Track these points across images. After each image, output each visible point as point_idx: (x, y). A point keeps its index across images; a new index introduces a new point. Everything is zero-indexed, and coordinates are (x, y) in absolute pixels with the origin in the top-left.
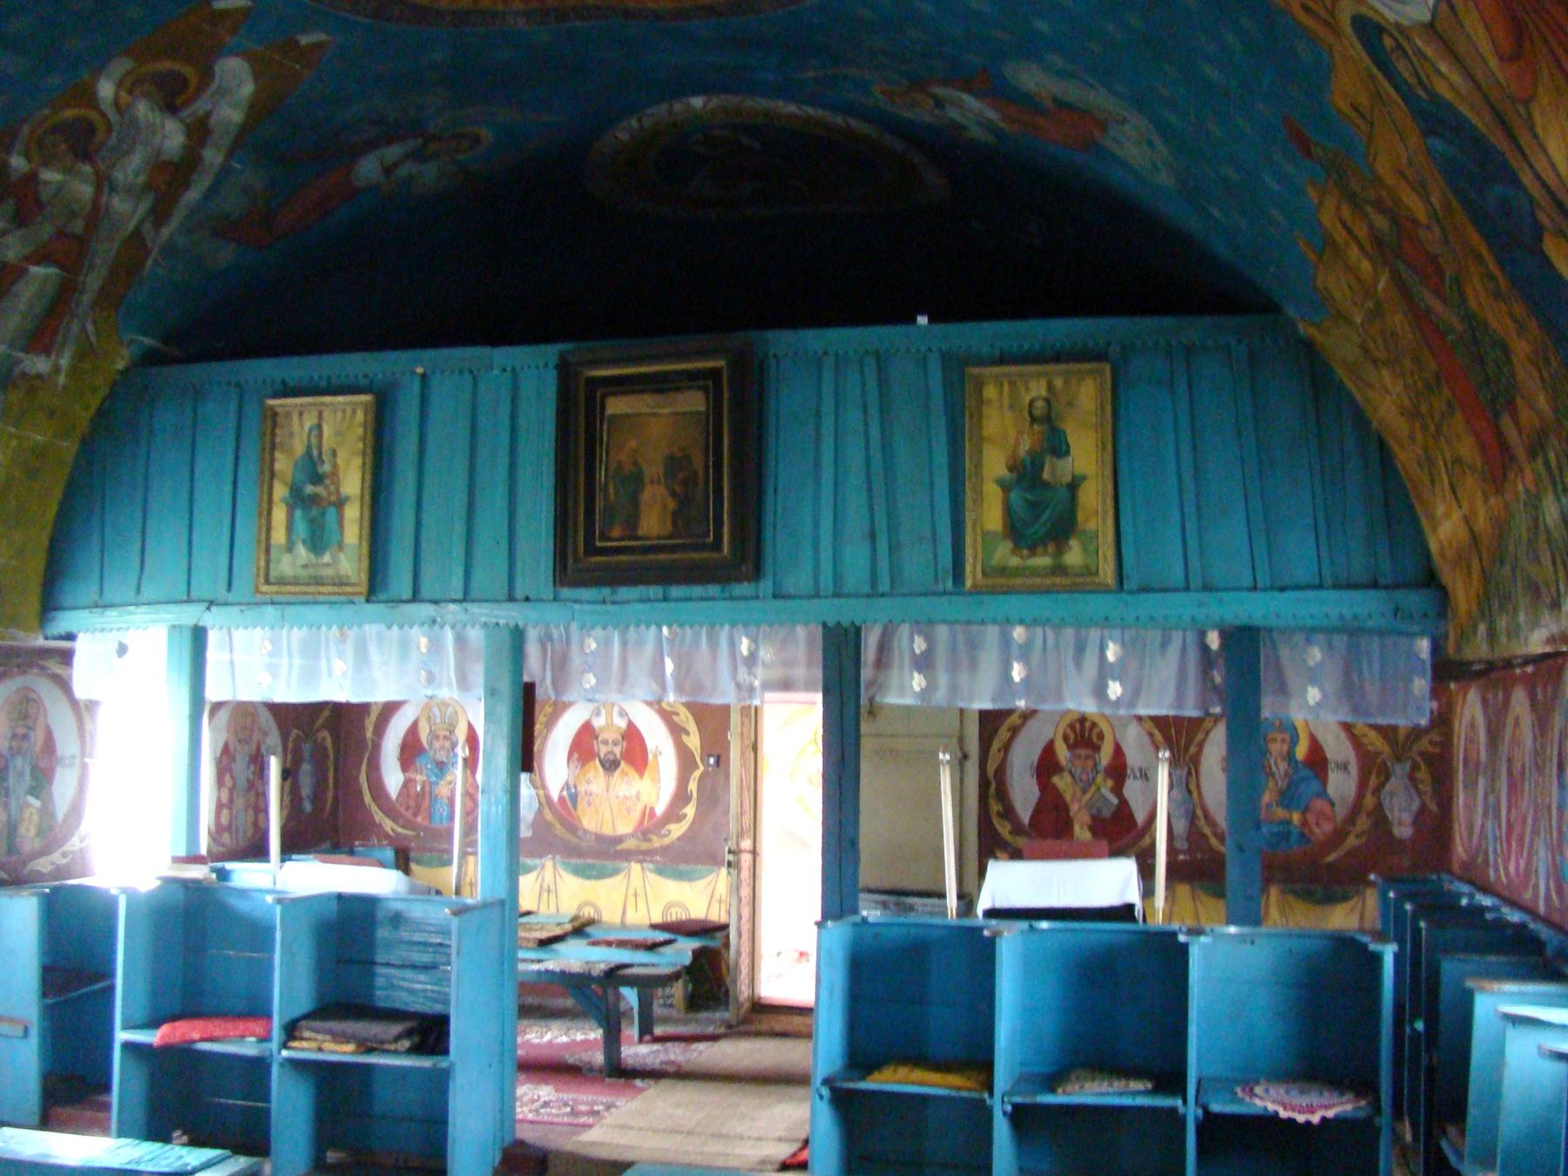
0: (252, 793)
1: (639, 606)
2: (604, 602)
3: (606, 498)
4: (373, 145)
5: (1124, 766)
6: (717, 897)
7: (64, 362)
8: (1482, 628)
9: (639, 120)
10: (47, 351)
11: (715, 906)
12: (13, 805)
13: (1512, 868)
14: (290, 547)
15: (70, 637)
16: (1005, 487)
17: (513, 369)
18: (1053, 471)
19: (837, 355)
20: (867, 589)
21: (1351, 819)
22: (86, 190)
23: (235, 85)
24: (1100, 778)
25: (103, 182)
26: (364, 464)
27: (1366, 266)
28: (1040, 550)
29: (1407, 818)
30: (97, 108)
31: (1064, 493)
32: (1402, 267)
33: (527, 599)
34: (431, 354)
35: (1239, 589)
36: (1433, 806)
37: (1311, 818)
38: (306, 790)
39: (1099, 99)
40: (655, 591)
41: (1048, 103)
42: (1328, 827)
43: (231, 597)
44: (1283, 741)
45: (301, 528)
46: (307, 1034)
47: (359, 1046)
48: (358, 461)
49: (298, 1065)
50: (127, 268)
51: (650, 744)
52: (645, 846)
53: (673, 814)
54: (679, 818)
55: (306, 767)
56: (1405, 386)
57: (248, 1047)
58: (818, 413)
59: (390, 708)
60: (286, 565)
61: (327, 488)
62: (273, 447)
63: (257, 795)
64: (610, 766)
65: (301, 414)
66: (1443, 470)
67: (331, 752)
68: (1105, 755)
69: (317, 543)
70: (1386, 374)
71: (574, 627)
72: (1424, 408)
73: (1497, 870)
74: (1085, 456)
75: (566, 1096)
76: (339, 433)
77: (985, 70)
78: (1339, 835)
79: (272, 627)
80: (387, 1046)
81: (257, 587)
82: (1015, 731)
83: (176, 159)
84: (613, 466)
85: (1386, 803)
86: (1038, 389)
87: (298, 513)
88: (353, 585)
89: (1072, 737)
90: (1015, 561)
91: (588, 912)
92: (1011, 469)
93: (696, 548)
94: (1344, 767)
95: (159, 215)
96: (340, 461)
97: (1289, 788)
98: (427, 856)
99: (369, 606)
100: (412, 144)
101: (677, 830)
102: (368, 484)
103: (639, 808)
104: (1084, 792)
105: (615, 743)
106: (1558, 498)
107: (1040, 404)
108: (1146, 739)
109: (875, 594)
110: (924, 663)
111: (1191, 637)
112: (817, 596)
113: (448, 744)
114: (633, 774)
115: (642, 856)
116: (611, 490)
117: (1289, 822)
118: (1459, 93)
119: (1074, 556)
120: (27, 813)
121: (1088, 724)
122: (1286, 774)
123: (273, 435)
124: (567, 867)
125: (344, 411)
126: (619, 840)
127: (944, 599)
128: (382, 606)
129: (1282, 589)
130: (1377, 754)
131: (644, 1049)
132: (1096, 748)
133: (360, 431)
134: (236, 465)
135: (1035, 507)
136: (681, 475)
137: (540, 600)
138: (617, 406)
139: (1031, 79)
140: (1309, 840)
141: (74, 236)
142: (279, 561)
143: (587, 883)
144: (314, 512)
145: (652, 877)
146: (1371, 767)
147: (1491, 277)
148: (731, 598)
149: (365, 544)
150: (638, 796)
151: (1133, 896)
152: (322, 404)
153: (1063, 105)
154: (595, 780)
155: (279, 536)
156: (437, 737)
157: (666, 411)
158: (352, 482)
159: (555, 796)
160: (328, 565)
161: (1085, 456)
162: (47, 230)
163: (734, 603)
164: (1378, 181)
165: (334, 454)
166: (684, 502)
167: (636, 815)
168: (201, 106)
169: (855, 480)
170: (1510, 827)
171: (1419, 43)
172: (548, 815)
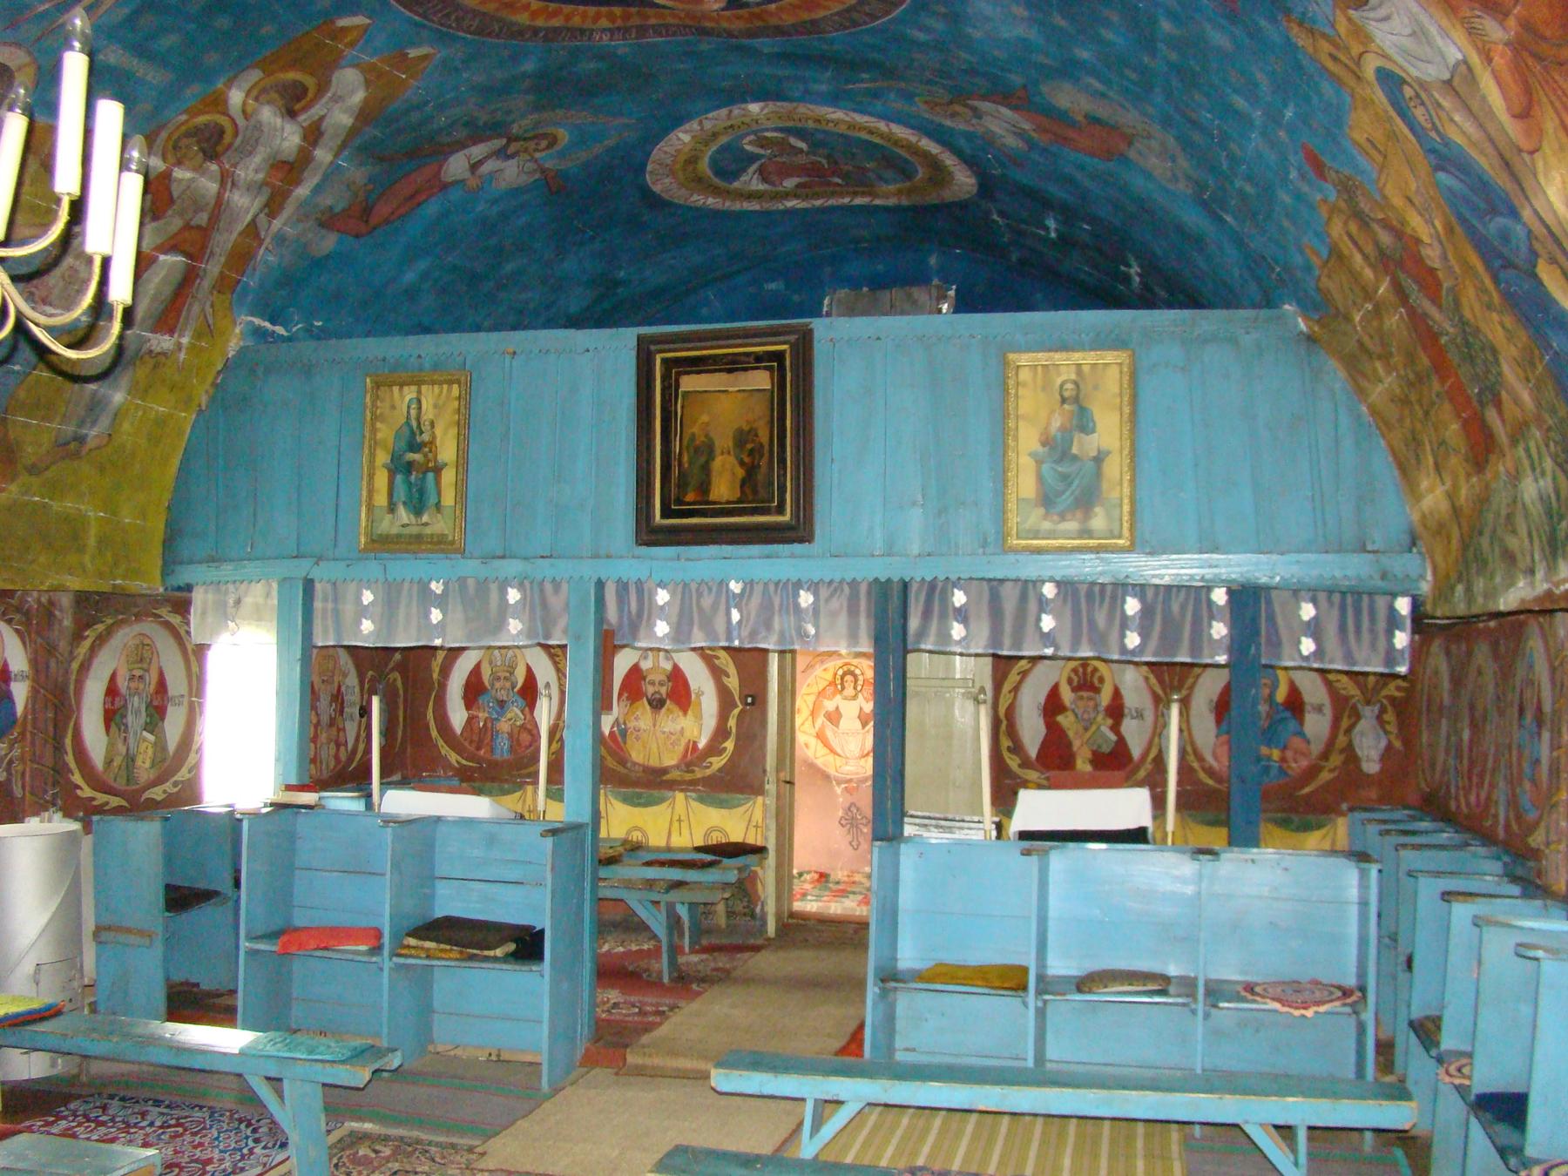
0: (334, 729)
3: (680, 465)
4: (461, 145)
7: (185, 341)
8: (1460, 588)
9: (701, 123)
10: (171, 332)
11: (752, 831)
12: (131, 741)
13: (1473, 798)
14: (392, 508)
15: (189, 588)
16: (1039, 462)
21: (1325, 756)
22: (213, 187)
23: (347, 95)
24: (1100, 718)
25: (226, 179)
27: (1368, 274)
28: (1069, 516)
29: (1375, 754)
30: (226, 113)
32: (1402, 276)
36: (1397, 744)
37: (1289, 754)
39: (1129, 118)
41: (1080, 118)
42: (1304, 763)
50: (241, 258)
51: (693, 686)
52: (688, 777)
53: (714, 748)
54: (721, 752)
56: (1398, 376)
59: (455, 653)
63: (339, 730)
64: (657, 704)
66: (1428, 448)
68: (1105, 697)
70: (1378, 365)
72: (1413, 398)
73: (1457, 799)
74: (1108, 432)
75: (632, 999)
77: (1025, 87)
78: (1312, 772)
82: (1024, 674)
83: (291, 159)
85: (1356, 742)
89: (1076, 679)
91: (636, 836)
92: (1044, 444)
95: (273, 207)
100: (498, 143)
101: (717, 762)
103: (683, 742)
104: (1086, 729)
105: (661, 684)
106: (1536, 480)
107: (1069, 386)
113: (508, 685)
114: (678, 712)
115: (686, 786)
116: (685, 458)
117: (1269, 758)
118: (1469, 138)
119: (1098, 522)
120: (143, 746)
121: (1089, 669)
126: (665, 771)
130: (1346, 699)
131: (695, 958)
132: (1097, 690)
136: (749, 446)
138: (689, 383)
139: (1067, 98)
140: (1286, 774)
141: (199, 227)
143: (637, 810)
145: (694, 804)
146: (1344, 710)
147: (1486, 291)
150: (682, 731)
153: (1094, 121)
154: (643, 717)
156: (499, 679)
159: (607, 731)
161: (1108, 432)
162: (176, 224)
164: (1386, 204)
165: (432, 424)
166: (751, 470)
167: (680, 749)
168: (317, 111)
170: (1472, 764)
171: (1437, 95)
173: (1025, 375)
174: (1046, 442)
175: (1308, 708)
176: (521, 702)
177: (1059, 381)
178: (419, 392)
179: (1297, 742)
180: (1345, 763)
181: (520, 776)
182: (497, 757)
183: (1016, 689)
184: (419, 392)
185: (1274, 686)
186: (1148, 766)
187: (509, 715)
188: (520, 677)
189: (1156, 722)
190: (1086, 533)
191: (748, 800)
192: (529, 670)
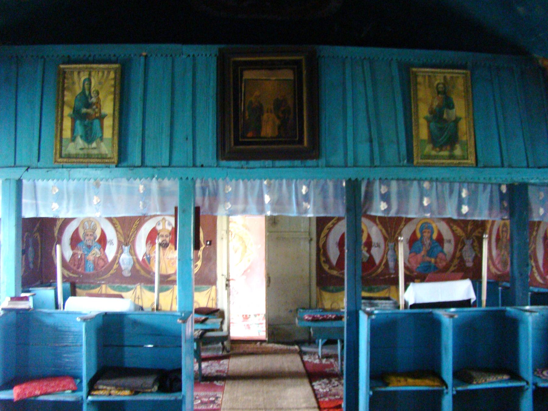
1: (260, 170)
2: (242, 168)
3: (244, 117)
5: (371, 242)
6: (211, 298)
14: (73, 139)
16: (429, 122)
17: (194, 55)
18: (448, 114)
19: (351, 58)
20: (368, 164)
26: (115, 99)
28: (444, 148)
29: (471, 259)
31: (452, 124)
33: (202, 166)
34: (152, 47)
35: (522, 167)
37: (438, 260)
38: (31, 259)
40: (268, 163)
42: (444, 264)
43: (39, 165)
44: (428, 232)
45: (80, 129)
46: (101, 387)
47: (131, 391)
48: (111, 97)
49: (93, 403)
55: (31, 249)
57: (68, 396)
58: (344, 84)
59: (67, 221)
60: (71, 148)
61: (94, 110)
62: (63, 90)
65: (79, 73)
67: (39, 242)
69: (89, 137)
71: (221, 182)
74: (460, 109)
76: (100, 83)
79: (58, 180)
80: (147, 390)
81: (55, 159)
84: (247, 105)
85: (464, 254)
86: (439, 80)
87: (78, 122)
88: (109, 158)
90: (433, 153)
93: (290, 143)
94: (449, 241)
96: (101, 96)
97: (430, 249)
98: (83, 285)
99: (117, 169)
102: (117, 108)
107: (441, 86)
108: (379, 232)
109: (372, 165)
110: (386, 198)
111: (495, 188)
112: (346, 166)
113: (92, 238)
117: (430, 262)
119: (458, 152)
122: (430, 244)
123: (64, 83)
124: (146, 288)
125: (103, 73)
126: (169, 276)
127: (404, 169)
128: (125, 169)
129: (539, 168)
130: (460, 237)
133: (113, 82)
134: (42, 98)
135: (441, 130)
136: (282, 109)
137: (210, 167)
138: (248, 75)
142: (67, 146)
144: (86, 122)
148: (305, 167)
149: (116, 138)
151: (473, 297)
152: (92, 68)
155: (67, 134)
156: (88, 235)
157: (274, 78)
158: (108, 107)
159: (141, 259)
160: (95, 148)
163: (308, 169)
165: (98, 93)
169: (362, 115)
172: (138, 267)
173: (420, 79)
174: (431, 112)
175: (445, 241)
176: (99, 246)
177: (436, 83)
178: (90, 75)
179: (441, 255)
180: (459, 263)
181: (99, 280)
182: (87, 272)
183: (327, 235)
184: (90, 75)
185: (432, 232)
186: (382, 267)
187: (93, 252)
188: (98, 234)
189: (385, 248)
190: (452, 157)
191: (208, 288)
192: (103, 231)
